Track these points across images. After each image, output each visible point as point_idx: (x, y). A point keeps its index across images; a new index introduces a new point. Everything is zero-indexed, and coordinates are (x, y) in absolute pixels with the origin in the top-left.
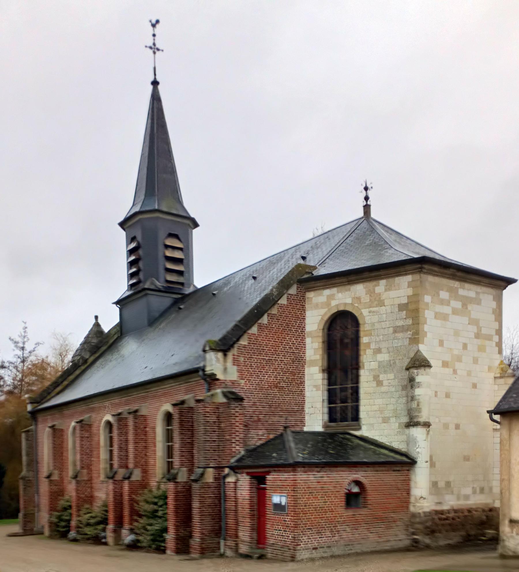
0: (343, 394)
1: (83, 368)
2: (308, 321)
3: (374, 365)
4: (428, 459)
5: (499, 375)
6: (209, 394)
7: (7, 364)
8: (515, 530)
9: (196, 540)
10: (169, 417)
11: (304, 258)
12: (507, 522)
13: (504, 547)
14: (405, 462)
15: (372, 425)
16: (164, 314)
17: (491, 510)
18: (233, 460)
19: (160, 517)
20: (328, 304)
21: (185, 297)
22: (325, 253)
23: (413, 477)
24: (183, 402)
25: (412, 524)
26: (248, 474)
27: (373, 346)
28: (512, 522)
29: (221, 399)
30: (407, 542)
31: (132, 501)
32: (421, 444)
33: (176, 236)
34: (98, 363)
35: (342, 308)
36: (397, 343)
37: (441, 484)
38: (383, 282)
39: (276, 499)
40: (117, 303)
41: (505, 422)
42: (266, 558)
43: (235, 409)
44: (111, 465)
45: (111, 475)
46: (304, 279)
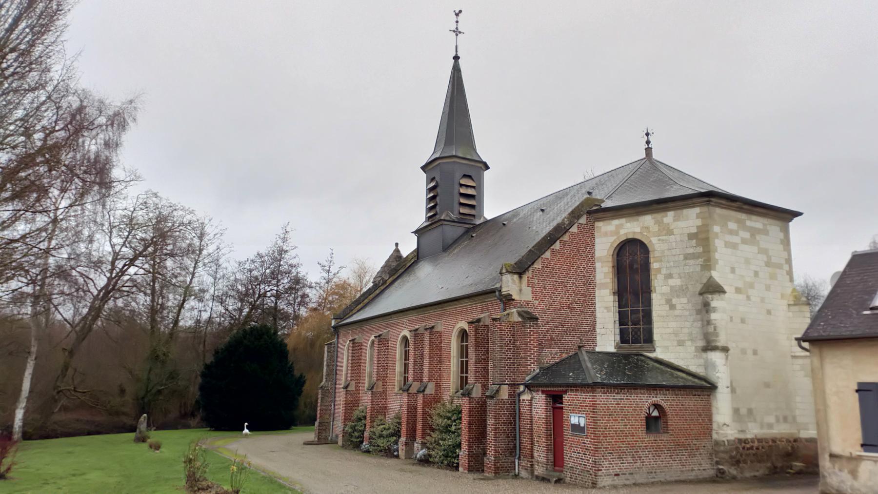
0: (634, 316)
1: (382, 288)
2: (597, 247)
3: (666, 289)
4: (729, 385)
5: (792, 303)
6: (506, 313)
7: (314, 285)
8: (837, 466)
9: (490, 458)
10: (463, 335)
11: (589, 193)
12: (827, 456)
13: (826, 484)
14: (705, 388)
15: (667, 348)
16: (456, 241)
17: (795, 441)
18: (527, 378)
19: (454, 433)
20: (617, 232)
21: (475, 227)
22: (611, 189)
23: (714, 403)
24: (479, 320)
25: (717, 453)
26: (543, 392)
27: (664, 271)
28: (832, 456)
29: (516, 318)
30: (711, 472)
31: (424, 413)
32: (720, 369)
33: (470, 177)
34: (396, 283)
35: (630, 236)
36: (687, 269)
37: (743, 411)
38: (671, 214)
39: (574, 420)
40: (415, 232)
41: (816, 350)
42: (564, 482)
43: (530, 327)
44: (406, 379)
45: (406, 388)
46: (593, 211)
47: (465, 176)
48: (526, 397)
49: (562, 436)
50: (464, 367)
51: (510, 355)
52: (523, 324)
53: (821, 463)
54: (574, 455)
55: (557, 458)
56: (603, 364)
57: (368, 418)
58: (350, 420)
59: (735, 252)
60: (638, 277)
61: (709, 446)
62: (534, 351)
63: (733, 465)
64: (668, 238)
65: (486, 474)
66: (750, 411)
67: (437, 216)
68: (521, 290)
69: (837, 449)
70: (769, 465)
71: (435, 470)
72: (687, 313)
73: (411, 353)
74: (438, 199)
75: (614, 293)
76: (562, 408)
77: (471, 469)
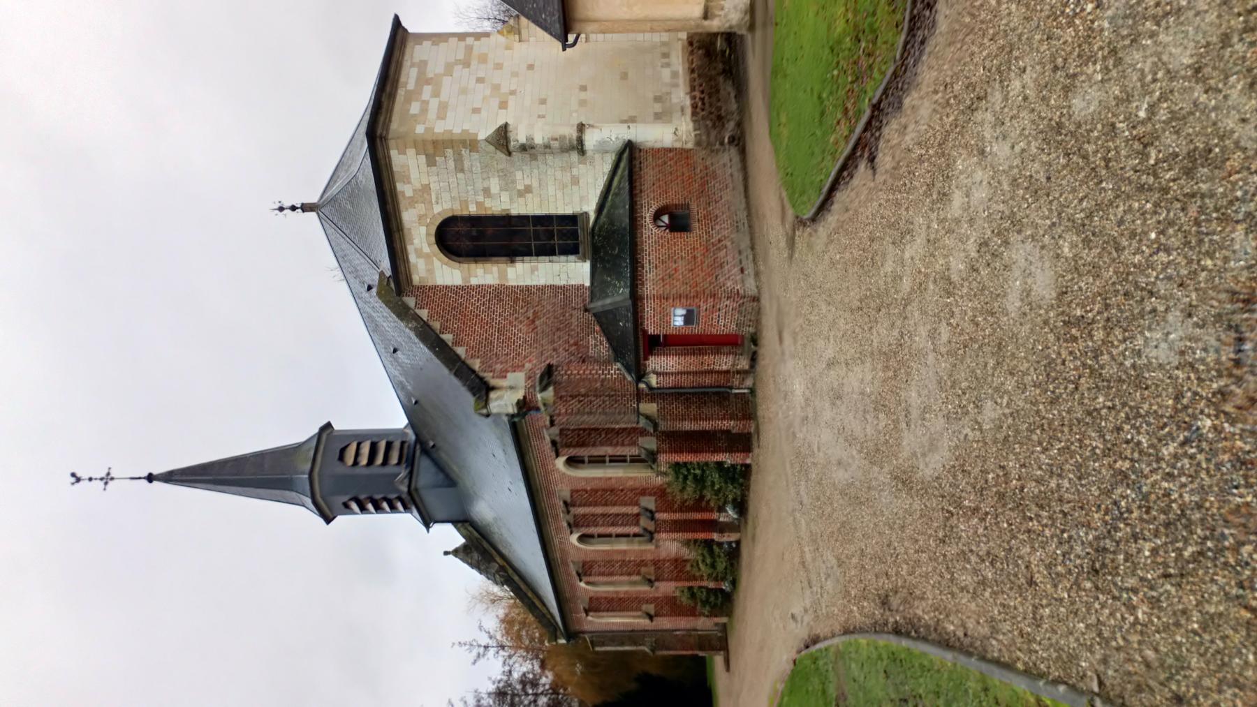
1: (510, 571)
3: (505, 197)
6: (543, 408)
7: (507, 668)
8: (717, 13)
10: (573, 462)
11: (370, 288)
12: (706, 23)
13: (739, 26)
14: (630, 154)
15: (582, 199)
16: (440, 467)
17: (691, 44)
18: (629, 379)
19: (703, 471)
20: (427, 257)
21: (419, 440)
23: (649, 145)
24: (554, 443)
26: (646, 359)
27: (481, 198)
28: (706, 16)
29: (550, 393)
32: (606, 136)
33: (343, 451)
34: (504, 551)
36: (477, 167)
37: (658, 108)
38: (400, 187)
39: (679, 321)
40: (427, 526)
41: (577, 26)
43: (561, 376)
46: (397, 287)
47: (341, 458)
48: (653, 380)
49: (700, 336)
50: (618, 460)
51: (598, 401)
52: (557, 384)
53: (715, 30)
54: (722, 322)
55: (727, 343)
56: (606, 282)
57: (691, 584)
58: (695, 608)
59: (447, 106)
60: (490, 230)
61: (703, 153)
62: (593, 370)
63: (723, 125)
64: (431, 194)
65: (752, 430)
66: (657, 99)
67: (404, 496)
68: (511, 388)
69: (697, 11)
70: (721, 79)
71: (752, 495)
72: (536, 171)
73: (601, 530)
74: (378, 497)
75: (513, 262)
76: (665, 336)
77: (747, 449)
